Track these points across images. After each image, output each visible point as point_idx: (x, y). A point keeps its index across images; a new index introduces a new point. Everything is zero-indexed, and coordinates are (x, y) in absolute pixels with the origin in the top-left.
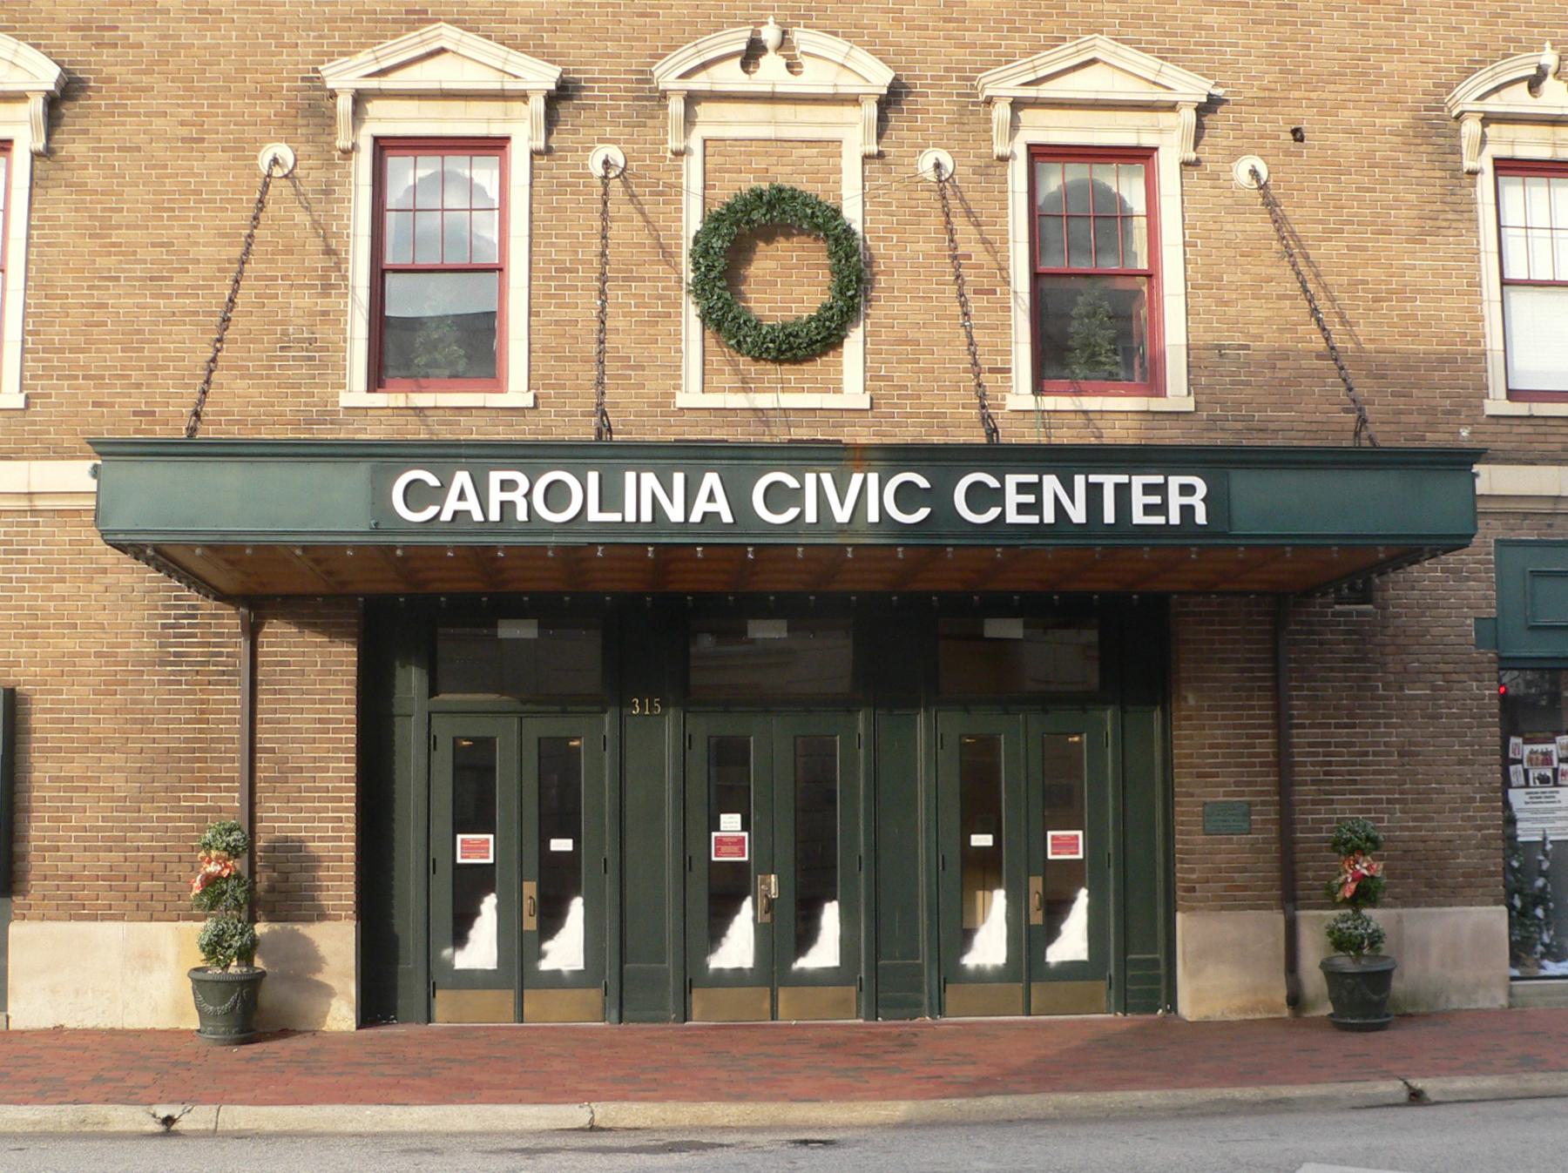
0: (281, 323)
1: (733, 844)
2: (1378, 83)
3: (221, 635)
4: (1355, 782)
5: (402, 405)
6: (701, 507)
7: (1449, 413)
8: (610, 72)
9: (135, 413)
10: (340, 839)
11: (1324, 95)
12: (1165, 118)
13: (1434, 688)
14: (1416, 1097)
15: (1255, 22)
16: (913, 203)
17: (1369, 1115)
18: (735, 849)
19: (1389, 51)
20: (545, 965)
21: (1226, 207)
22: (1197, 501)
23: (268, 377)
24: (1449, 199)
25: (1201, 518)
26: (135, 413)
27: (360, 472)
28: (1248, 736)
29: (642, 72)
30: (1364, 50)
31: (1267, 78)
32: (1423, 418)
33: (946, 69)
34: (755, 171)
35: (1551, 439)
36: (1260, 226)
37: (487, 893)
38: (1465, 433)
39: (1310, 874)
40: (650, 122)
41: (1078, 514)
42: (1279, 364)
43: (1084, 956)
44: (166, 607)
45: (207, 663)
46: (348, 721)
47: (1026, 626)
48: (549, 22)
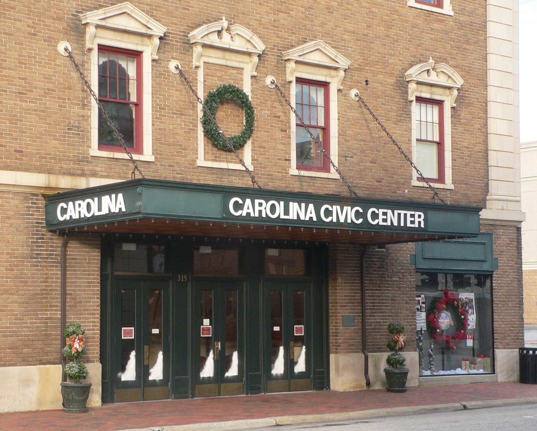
0: (66, 118)
1: (207, 330)
2: (388, 66)
3: (52, 247)
4: (380, 309)
5: (112, 157)
6: (308, 215)
7: (402, 184)
8: (175, 30)
9: (15, 151)
10: (94, 330)
11: (374, 69)
12: (333, 73)
13: (400, 278)
14: (465, 408)
15: (357, 40)
16: (265, 95)
17: (458, 412)
18: (207, 332)
19: (391, 55)
20: (151, 378)
21: (348, 107)
22: (421, 219)
23: (64, 141)
24: (404, 110)
25: (422, 226)
26: (15, 151)
27: (218, 198)
28: (354, 293)
29: (185, 32)
30: (385, 54)
31: (361, 61)
32: (396, 186)
33: (274, 46)
34: (218, 77)
35: (428, 195)
36: (356, 115)
37: (132, 350)
38: (406, 191)
39: (369, 341)
40: (188, 53)
41: (396, 224)
42: (361, 164)
43: (304, 370)
44: (33, 234)
45: (47, 258)
46: (98, 283)
47: (212, 249)
48: (155, 6)
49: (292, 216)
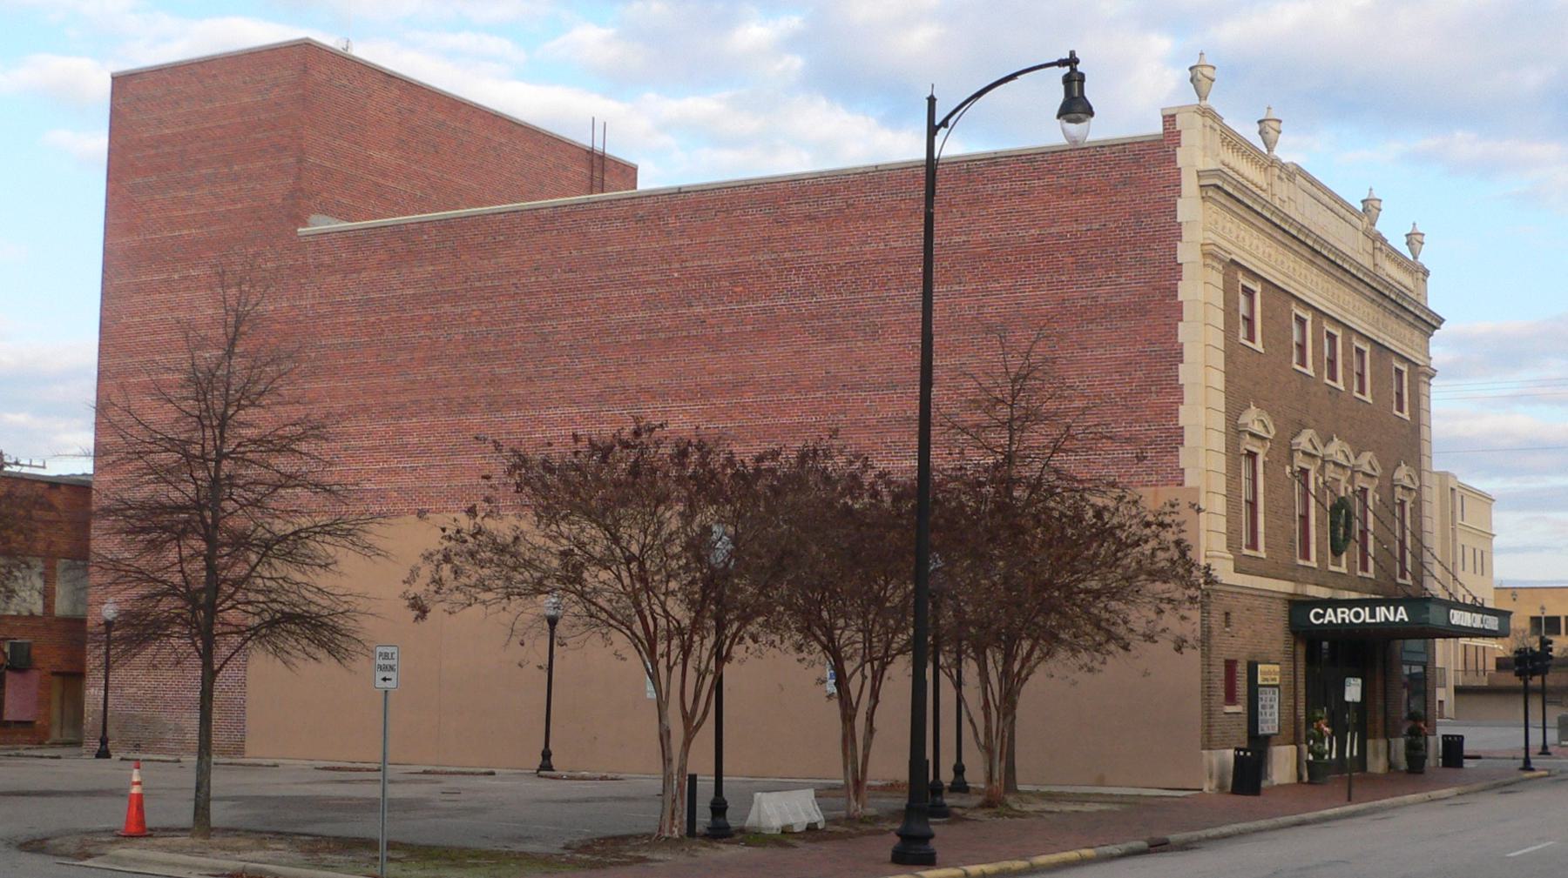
49: (1380, 618)
